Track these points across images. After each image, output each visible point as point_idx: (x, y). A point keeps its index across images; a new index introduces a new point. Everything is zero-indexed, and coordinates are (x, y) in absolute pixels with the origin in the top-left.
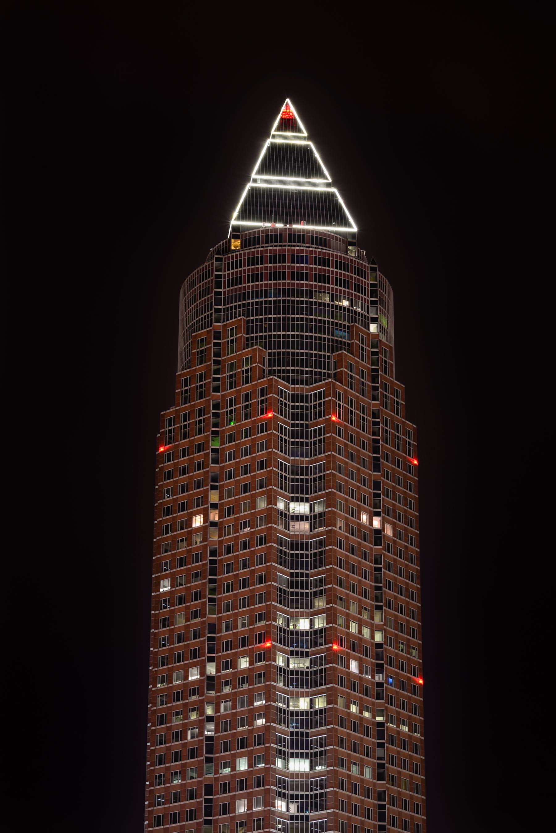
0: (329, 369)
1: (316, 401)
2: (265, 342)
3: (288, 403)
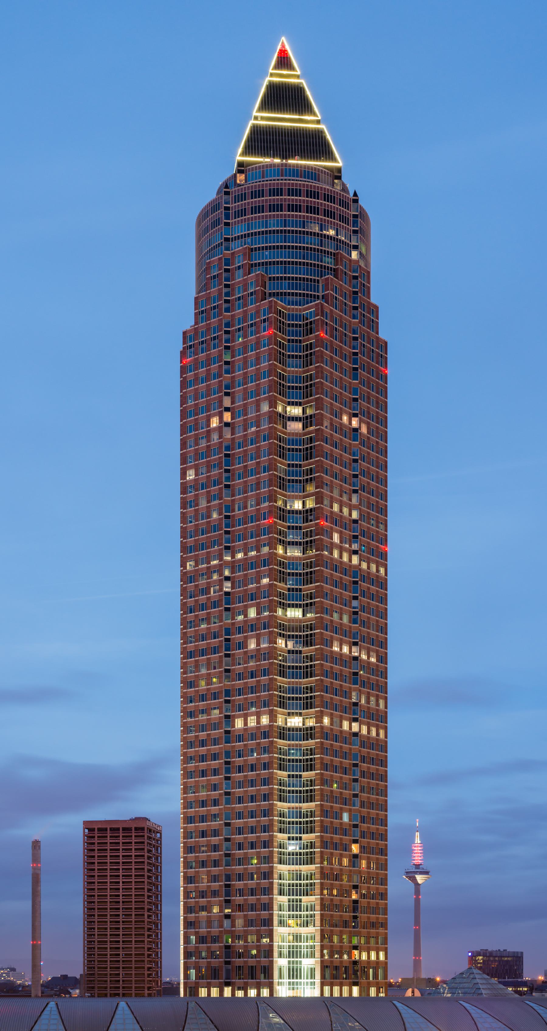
0: (318, 292)
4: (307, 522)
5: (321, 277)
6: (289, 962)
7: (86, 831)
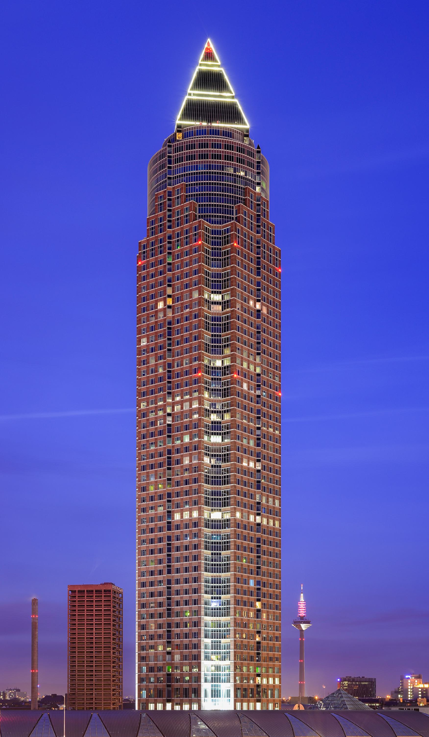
0: (233, 215)
1: (225, 234)
2: (197, 198)
3: (210, 235)
4: (225, 375)
5: (235, 204)
6: (212, 554)
7: (70, 592)
